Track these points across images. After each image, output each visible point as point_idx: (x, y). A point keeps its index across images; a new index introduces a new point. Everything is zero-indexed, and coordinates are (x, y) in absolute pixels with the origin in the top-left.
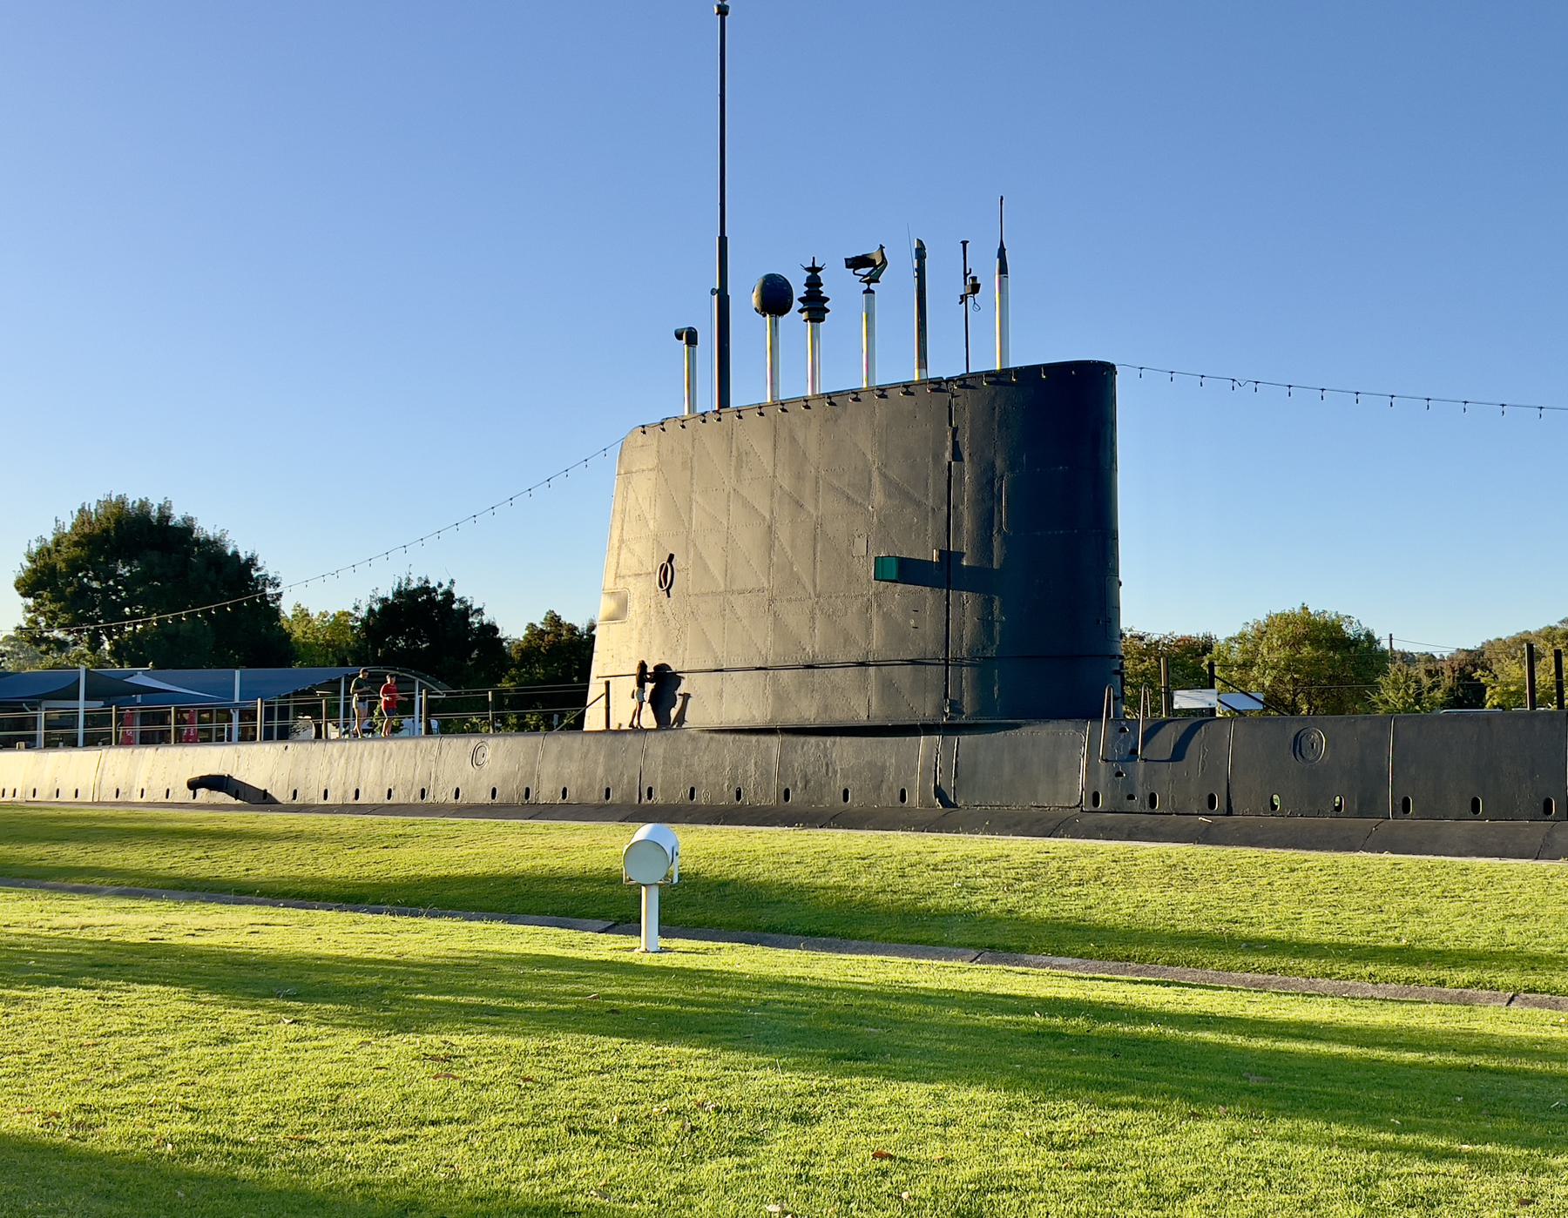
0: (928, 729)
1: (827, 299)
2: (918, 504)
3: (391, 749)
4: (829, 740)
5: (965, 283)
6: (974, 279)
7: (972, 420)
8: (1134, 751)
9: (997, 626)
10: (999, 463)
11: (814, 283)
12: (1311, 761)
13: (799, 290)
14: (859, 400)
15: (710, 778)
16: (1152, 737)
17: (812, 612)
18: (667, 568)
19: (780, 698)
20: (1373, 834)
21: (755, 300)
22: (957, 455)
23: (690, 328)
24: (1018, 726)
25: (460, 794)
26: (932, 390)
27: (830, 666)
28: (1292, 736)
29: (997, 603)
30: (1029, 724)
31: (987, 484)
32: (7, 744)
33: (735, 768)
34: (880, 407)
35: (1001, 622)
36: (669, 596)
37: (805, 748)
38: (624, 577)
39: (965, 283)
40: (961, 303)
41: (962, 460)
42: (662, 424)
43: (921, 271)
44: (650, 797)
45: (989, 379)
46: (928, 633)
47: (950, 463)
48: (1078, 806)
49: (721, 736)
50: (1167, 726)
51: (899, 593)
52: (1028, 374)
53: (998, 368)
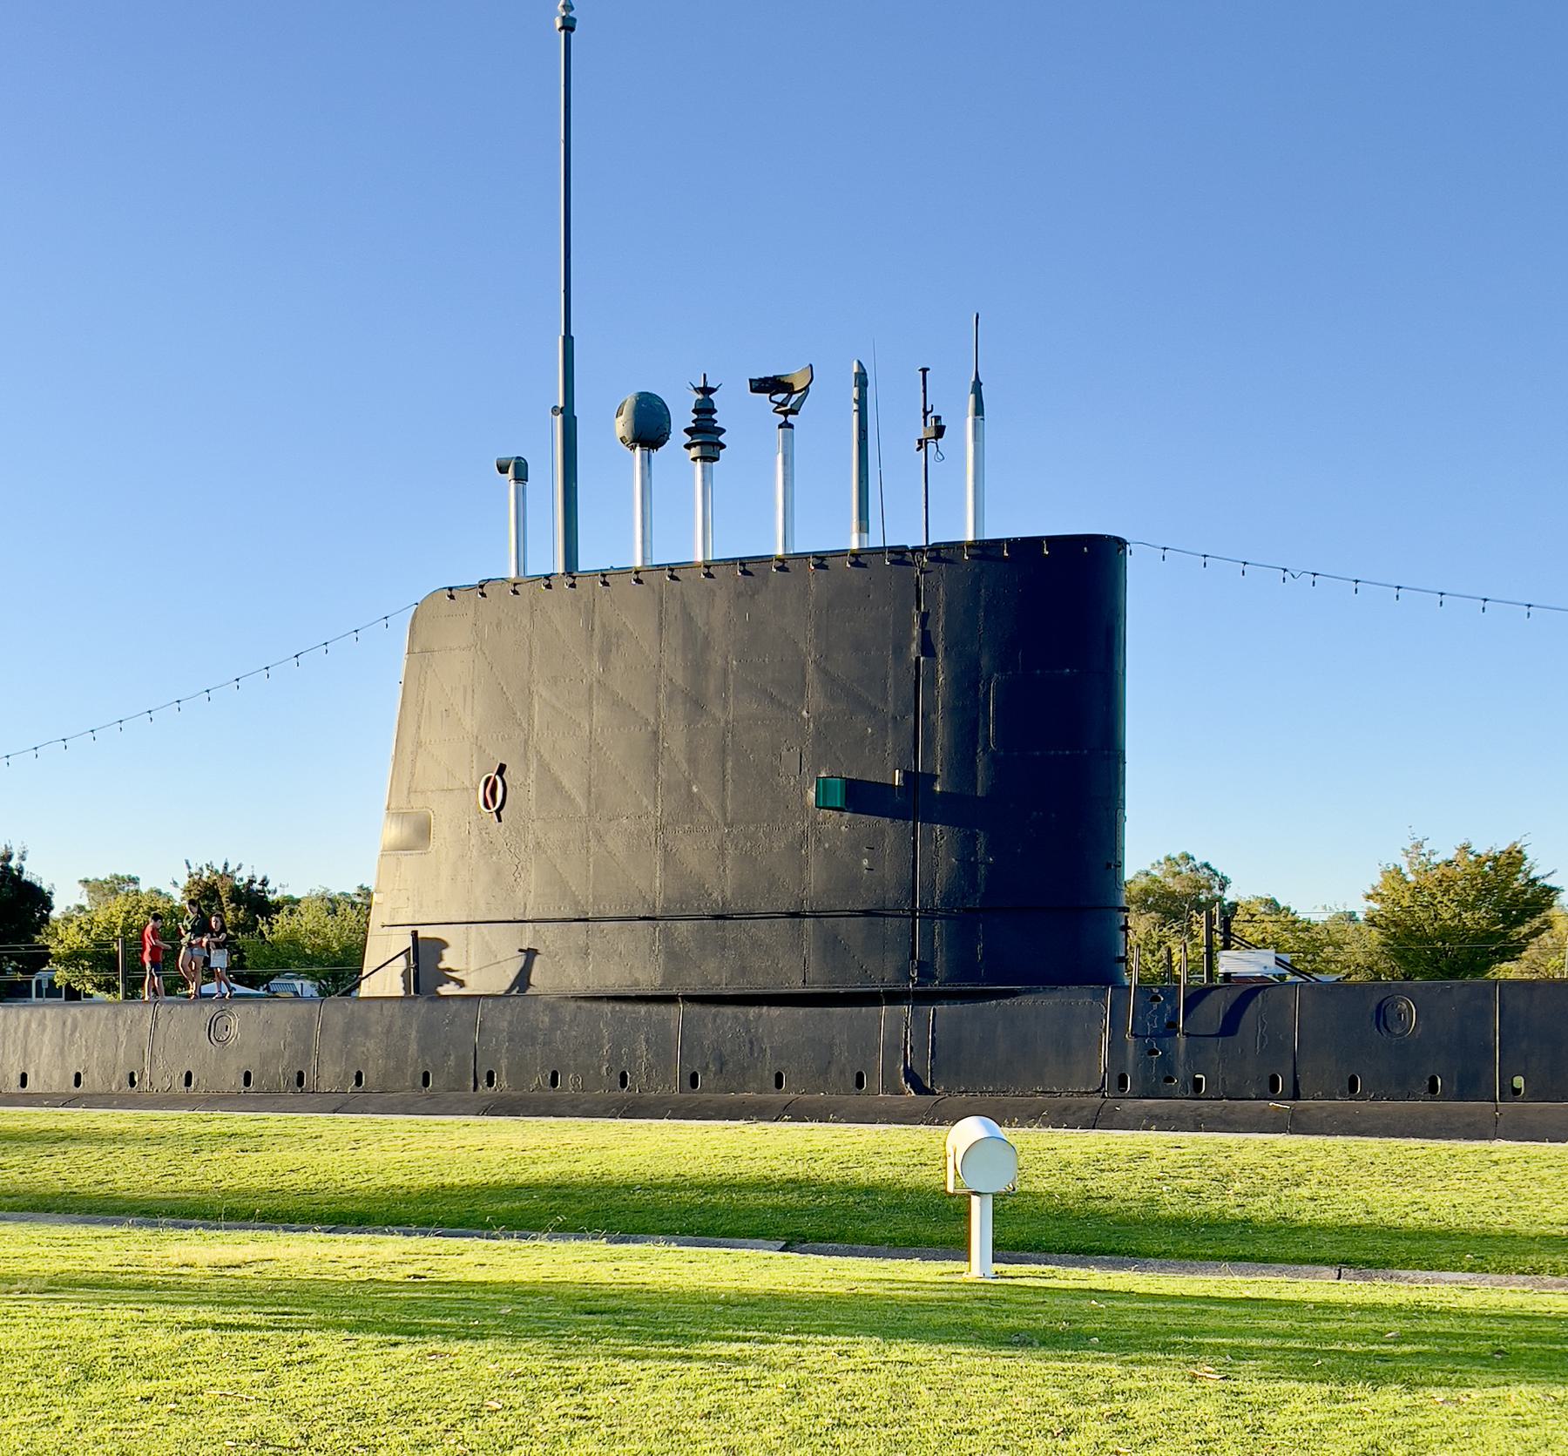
0: (894, 998)
1: (723, 431)
2: (874, 711)
3: (75, 1020)
4: (753, 1011)
5: (925, 424)
6: (938, 418)
7: (948, 605)
8: (1173, 1025)
9: (982, 870)
10: (985, 661)
11: (705, 410)
12: (1400, 1035)
13: (682, 417)
14: (787, 570)
15: (580, 1060)
16: (1196, 1005)
17: (722, 849)
18: (495, 782)
19: (674, 957)
20: (1501, 1119)
21: (622, 426)
22: (927, 648)
23: (518, 458)
24: (1014, 994)
25: (194, 1080)
26: (892, 562)
27: (750, 916)
28: (1373, 1007)
29: (981, 840)
30: (1029, 992)
31: (967, 683)
32: (14, 993)
33: (616, 1045)
34: (816, 582)
35: (988, 864)
36: (500, 820)
37: (718, 1021)
38: (422, 792)
39: (925, 424)
40: (918, 449)
41: (934, 655)
42: (481, 587)
43: (862, 402)
44: (490, 1083)
45: (973, 552)
46: (887, 876)
47: (918, 659)
48: (1099, 1091)
49: (595, 1005)
50: (1213, 993)
51: (841, 823)
52: (1026, 547)
53: (970, 537)
